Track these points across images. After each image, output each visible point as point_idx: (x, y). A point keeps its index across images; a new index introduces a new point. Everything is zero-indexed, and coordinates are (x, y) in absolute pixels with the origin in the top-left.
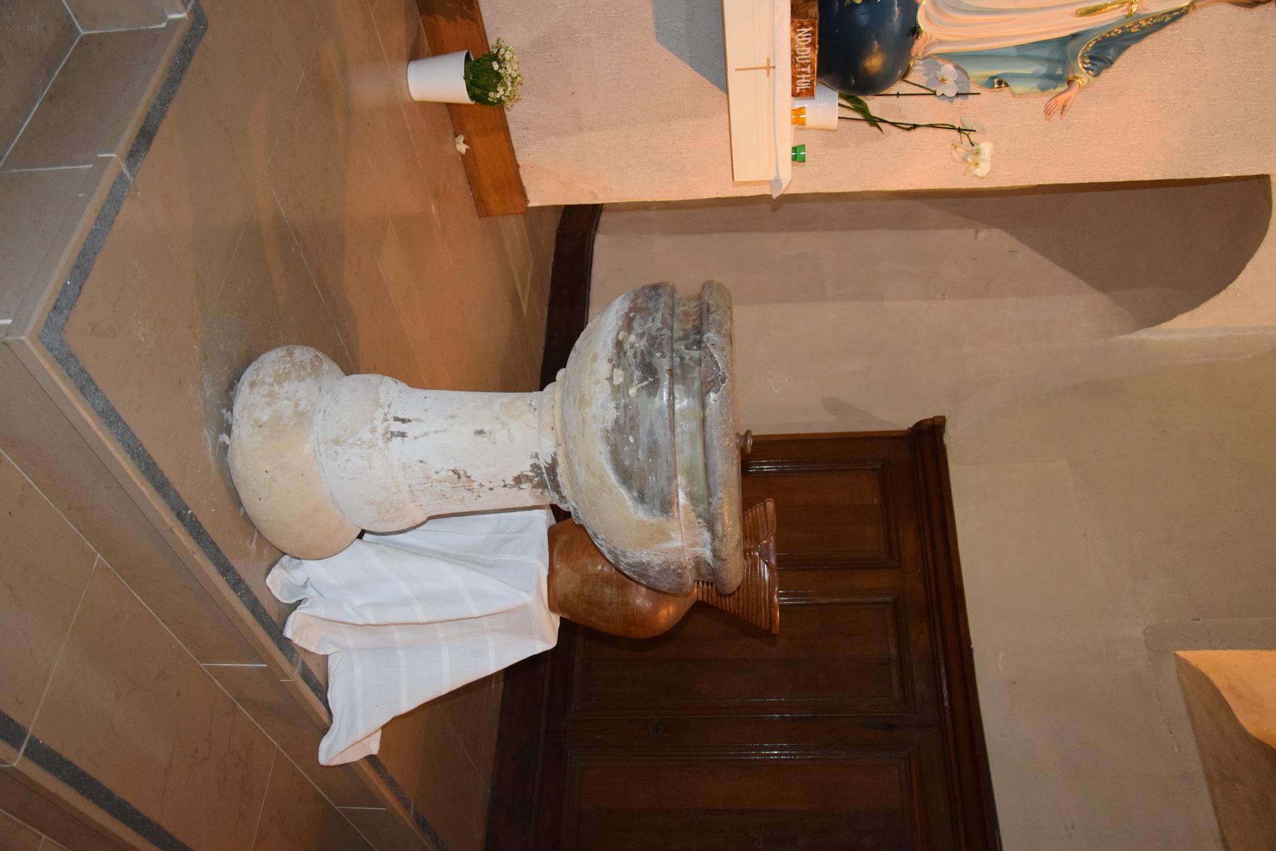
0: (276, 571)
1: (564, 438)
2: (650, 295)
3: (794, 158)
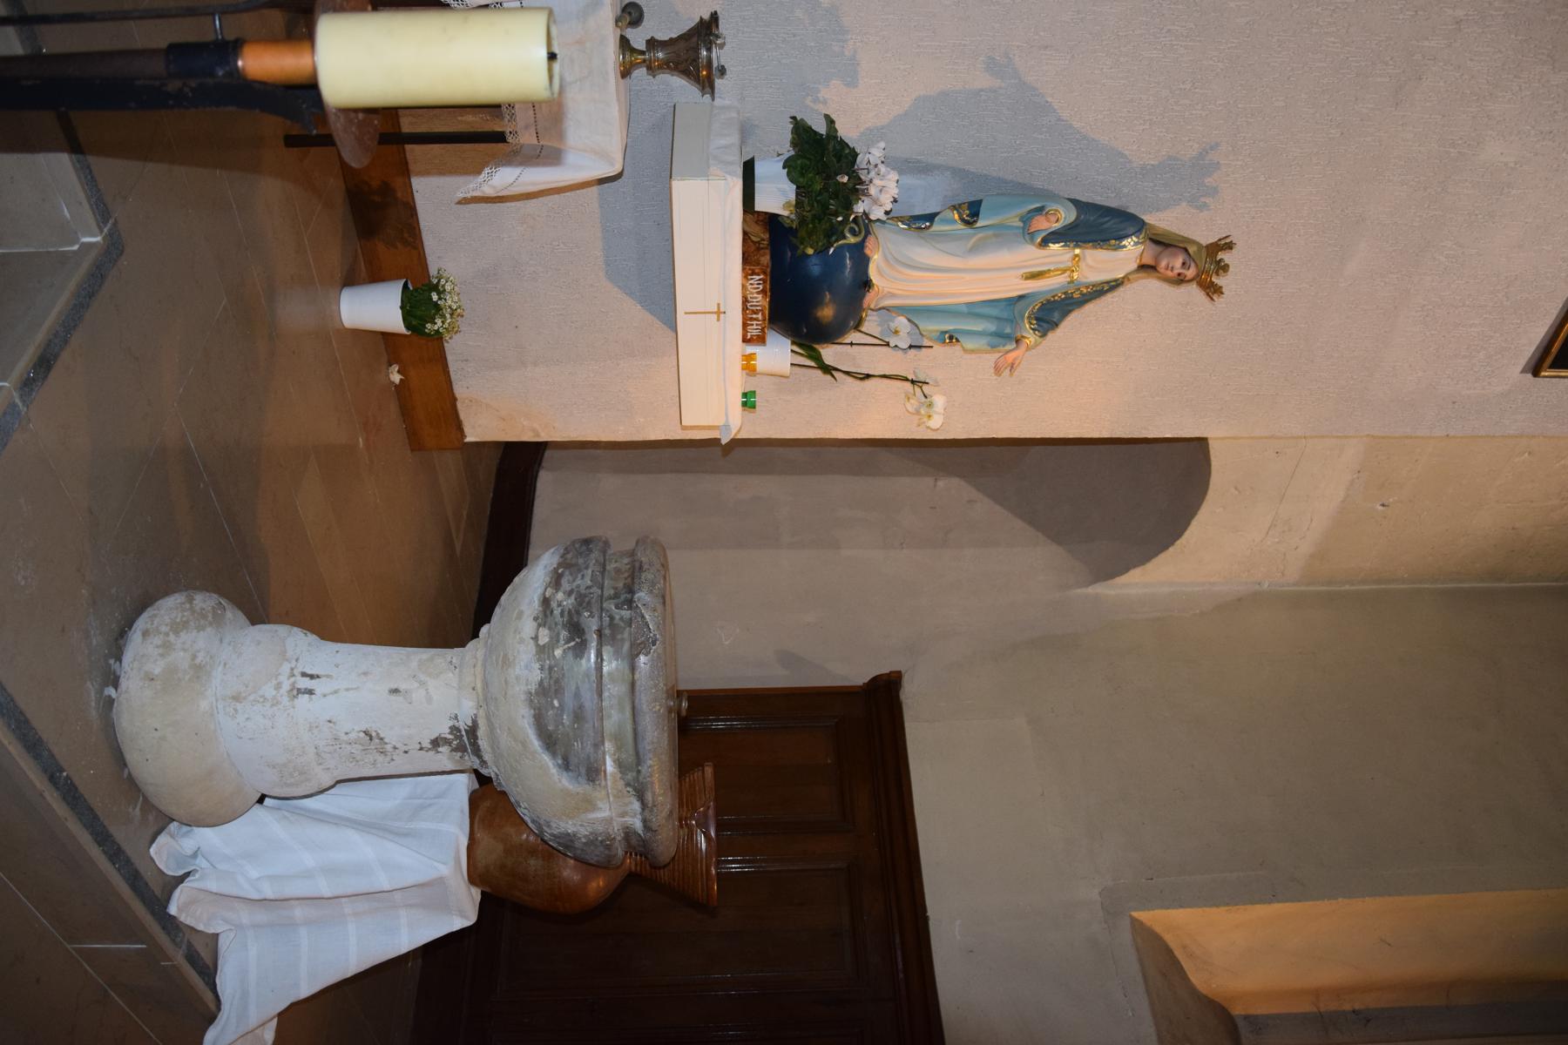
0: (162, 839)
1: (486, 699)
2: (582, 548)
3: (744, 404)
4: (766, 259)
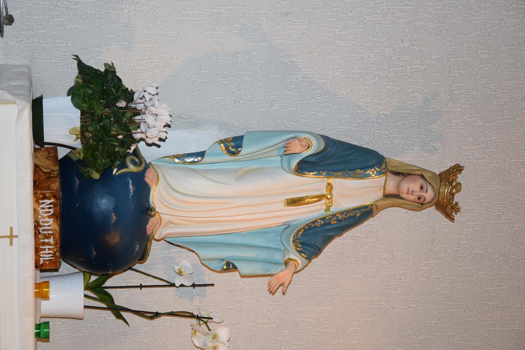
4: (56, 185)
